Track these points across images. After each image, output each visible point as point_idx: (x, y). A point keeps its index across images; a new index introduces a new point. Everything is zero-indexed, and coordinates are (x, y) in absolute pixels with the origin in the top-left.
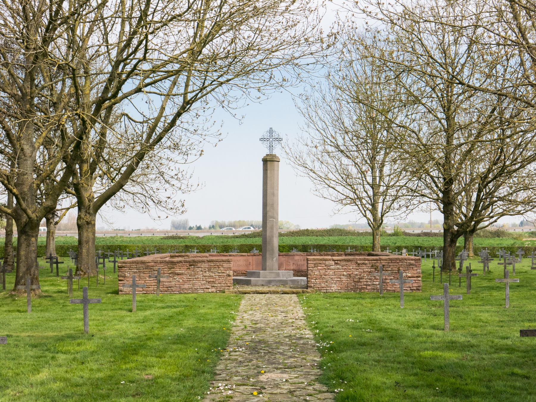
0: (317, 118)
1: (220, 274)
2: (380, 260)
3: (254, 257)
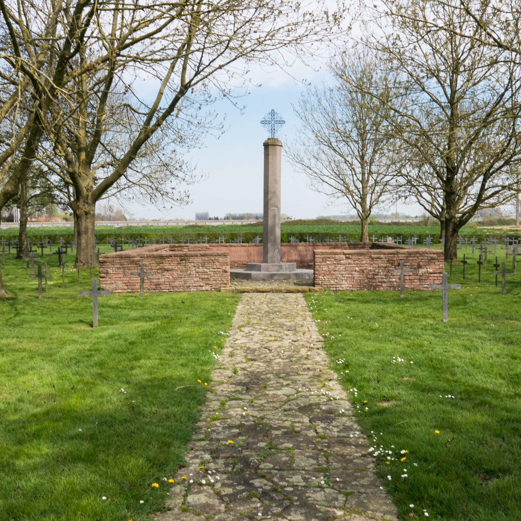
0: (314, 121)
1: (215, 270)
2: (398, 253)
3: (255, 248)
